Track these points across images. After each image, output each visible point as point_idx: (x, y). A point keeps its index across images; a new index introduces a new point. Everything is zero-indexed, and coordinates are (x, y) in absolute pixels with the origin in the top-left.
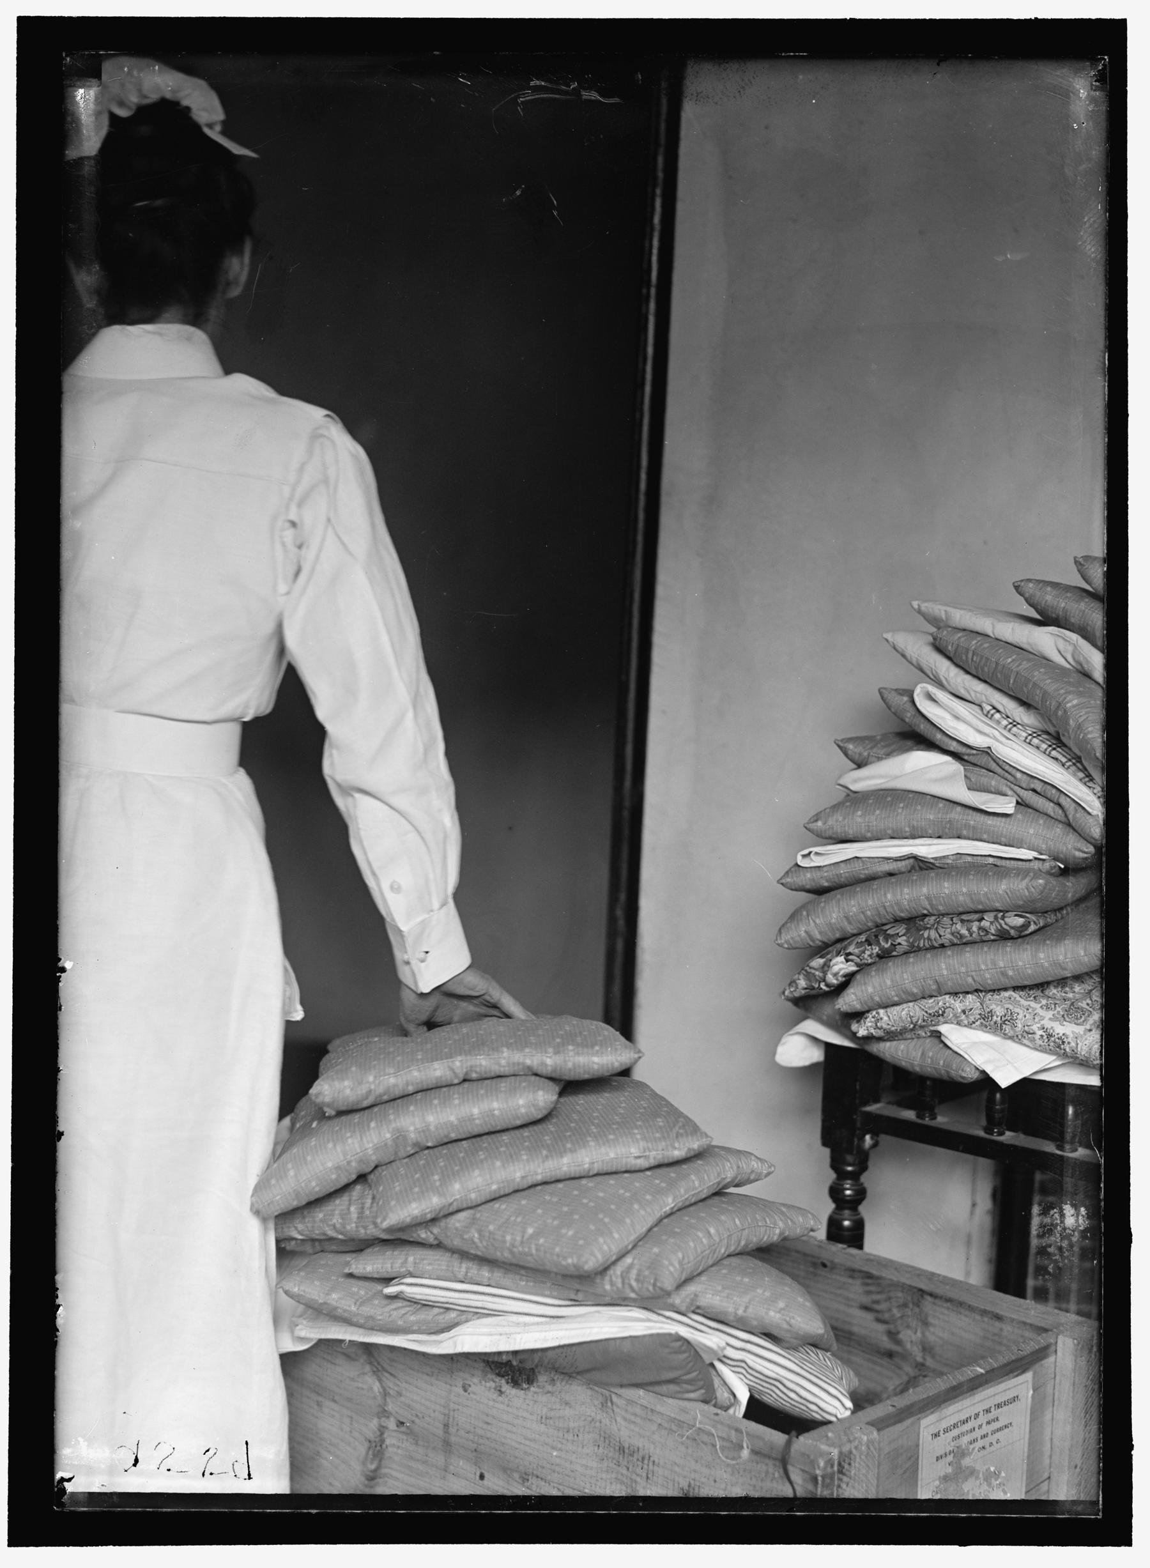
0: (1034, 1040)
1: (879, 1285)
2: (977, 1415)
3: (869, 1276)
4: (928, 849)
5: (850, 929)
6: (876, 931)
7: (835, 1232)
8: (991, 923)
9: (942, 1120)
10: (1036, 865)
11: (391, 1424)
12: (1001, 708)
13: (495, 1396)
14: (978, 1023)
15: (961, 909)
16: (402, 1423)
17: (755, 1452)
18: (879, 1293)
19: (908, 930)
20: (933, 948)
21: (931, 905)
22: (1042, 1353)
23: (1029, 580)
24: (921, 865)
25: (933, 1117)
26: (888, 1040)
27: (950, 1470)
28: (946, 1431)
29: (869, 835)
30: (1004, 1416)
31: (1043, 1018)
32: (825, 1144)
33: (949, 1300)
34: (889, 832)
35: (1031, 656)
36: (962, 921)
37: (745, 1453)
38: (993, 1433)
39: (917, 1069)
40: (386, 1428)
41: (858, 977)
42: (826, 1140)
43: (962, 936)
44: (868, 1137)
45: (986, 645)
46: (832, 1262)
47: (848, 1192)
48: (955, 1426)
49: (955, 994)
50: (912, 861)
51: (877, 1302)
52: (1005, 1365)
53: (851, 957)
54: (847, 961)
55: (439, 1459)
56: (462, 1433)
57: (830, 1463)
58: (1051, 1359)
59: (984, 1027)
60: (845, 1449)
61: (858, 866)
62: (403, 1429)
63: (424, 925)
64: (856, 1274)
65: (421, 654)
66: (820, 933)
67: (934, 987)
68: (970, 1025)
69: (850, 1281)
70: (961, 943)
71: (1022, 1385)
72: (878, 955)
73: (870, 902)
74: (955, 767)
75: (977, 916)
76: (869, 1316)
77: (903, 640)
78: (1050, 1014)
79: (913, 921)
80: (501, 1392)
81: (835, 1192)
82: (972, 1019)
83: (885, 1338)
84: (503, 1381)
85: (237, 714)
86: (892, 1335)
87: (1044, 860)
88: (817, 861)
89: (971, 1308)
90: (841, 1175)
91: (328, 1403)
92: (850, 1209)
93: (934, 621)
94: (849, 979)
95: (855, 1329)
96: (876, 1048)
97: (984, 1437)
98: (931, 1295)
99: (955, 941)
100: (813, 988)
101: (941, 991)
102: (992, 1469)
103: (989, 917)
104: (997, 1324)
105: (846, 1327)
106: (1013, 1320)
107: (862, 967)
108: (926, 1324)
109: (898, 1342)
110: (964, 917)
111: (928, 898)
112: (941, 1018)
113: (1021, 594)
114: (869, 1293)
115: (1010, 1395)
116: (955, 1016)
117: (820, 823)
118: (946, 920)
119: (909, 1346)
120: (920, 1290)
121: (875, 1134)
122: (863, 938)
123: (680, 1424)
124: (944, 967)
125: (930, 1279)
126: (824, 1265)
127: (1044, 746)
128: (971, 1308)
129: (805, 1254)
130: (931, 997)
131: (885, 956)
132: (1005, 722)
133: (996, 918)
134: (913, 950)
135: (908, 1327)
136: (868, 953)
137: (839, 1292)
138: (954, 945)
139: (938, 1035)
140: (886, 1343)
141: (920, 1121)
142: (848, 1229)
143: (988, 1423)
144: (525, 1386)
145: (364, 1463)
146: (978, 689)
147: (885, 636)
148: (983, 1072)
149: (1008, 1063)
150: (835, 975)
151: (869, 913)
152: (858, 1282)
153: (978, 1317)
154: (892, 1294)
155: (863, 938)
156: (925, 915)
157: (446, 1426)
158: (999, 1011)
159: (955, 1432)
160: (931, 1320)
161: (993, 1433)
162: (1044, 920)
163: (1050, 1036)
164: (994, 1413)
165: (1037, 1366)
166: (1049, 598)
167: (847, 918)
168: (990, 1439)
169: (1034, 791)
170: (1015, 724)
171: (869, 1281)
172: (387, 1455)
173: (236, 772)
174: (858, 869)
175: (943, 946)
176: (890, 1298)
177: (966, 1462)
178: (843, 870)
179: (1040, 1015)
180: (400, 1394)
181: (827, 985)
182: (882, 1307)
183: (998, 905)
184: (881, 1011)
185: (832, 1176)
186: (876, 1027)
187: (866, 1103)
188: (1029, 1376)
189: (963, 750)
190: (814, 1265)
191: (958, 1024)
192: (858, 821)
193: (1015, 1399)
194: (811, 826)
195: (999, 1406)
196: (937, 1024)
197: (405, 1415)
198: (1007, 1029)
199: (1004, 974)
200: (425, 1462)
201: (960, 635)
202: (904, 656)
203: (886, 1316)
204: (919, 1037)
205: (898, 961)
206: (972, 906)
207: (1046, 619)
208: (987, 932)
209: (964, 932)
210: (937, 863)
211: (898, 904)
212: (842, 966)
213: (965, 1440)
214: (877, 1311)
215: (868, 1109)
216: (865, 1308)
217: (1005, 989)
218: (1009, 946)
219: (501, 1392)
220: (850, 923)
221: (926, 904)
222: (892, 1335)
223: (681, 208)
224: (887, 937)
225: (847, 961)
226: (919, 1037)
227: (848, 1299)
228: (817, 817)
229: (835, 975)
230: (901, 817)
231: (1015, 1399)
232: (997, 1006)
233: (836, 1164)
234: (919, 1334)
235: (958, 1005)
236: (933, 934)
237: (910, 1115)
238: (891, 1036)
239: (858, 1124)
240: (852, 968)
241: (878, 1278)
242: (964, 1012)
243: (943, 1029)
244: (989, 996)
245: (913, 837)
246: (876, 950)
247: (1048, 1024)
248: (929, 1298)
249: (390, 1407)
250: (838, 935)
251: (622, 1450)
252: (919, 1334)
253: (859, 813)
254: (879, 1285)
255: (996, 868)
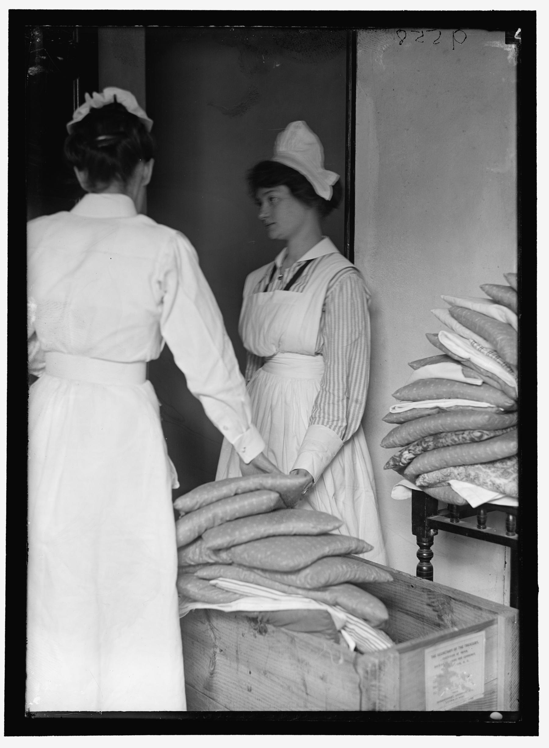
0: (487, 486)
1: (434, 595)
2: (455, 649)
3: (430, 591)
4: (444, 404)
5: (411, 439)
6: (421, 440)
7: (420, 572)
8: (468, 435)
9: (461, 523)
10: (489, 410)
11: (218, 651)
12: (476, 341)
13: (253, 638)
14: (464, 479)
15: (455, 430)
16: (222, 651)
17: (346, 661)
18: (434, 598)
19: (434, 439)
20: (444, 447)
21: (443, 428)
22: (490, 623)
23: (487, 285)
24: (441, 411)
25: (458, 522)
26: (431, 487)
27: (442, 672)
28: (439, 655)
29: (419, 398)
30: (470, 650)
31: (491, 476)
32: (414, 534)
33: (461, 601)
34: (427, 397)
35: (487, 318)
36: (456, 435)
37: (341, 661)
38: (465, 657)
39: (443, 500)
40: (216, 652)
41: (415, 460)
42: (415, 531)
43: (455, 441)
44: (432, 530)
45: (469, 314)
46: (415, 585)
47: (425, 555)
48: (444, 653)
49: (455, 466)
50: (437, 409)
51: (433, 602)
52: (469, 628)
53: (411, 451)
54: (409, 453)
55: (234, 665)
56: (242, 654)
57: (374, 665)
58: (495, 626)
59: (467, 481)
60: (382, 659)
61: (415, 412)
62: (222, 653)
63: (241, 440)
64: (425, 590)
65: (224, 328)
66: (399, 441)
67: (445, 464)
68: (462, 480)
69: (422, 593)
70: (456, 444)
71: (480, 637)
72: (422, 450)
73: (418, 427)
74: (459, 367)
75: (461, 432)
76: (431, 609)
77: (437, 312)
78: (494, 475)
79: (436, 435)
80: (255, 637)
81: (419, 555)
82: (462, 477)
83: (437, 618)
84: (256, 632)
85: (142, 358)
86: (440, 617)
87: (493, 407)
88: (398, 411)
89: (470, 605)
90: (422, 547)
91: (196, 642)
92: (425, 562)
93: (450, 303)
94: (411, 460)
95: (425, 614)
96: (431, 492)
97: (460, 658)
98: (454, 599)
99: (453, 443)
100: (396, 465)
101: (448, 466)
102: (465, 673)
103: (466, 433)
104: (480, 612)
105: (422, 613)
106: (486, 610)
107: (416, 456)
108: (452, 612)
109: (442, 620)
110: (457, 433)
111: (442, 425)
112: (449, 477)
113: (484, 290)
114: (430, 598)
115: (474, 640)
116: (455, 476)
117: (398, 394)
118: (449, 434)
119: (446, 622)
120: (450, 597)
121: (436, 529)
122: (416, 443)
123: (319, 649)
124: (448, 455)
125: (453, 592)
126: (412, 587)
127: (494, 357)
128: (470, 605)
129: (405, 582)
130: (445, 468)
131: (425, 450)
132: (478, 347)
133: (469, 433)
134: (436, 448)
135: (446, 613)
136: (417, 449)
137: (418, 598)
138: (453, 445)
139: (449, 485)
140: (437, 620)
141: (451, 523)
142: (425, 571)
143: (462, 652)
144: (264, 634)
145: (209, 668)
146: (467, 333)
147: (432, 311)
148: (466, 501)
149: (474, 495)
150: (405, 459)
151: (418, 432)
152: (426, 594)
153: (472, 609)
154: (439, 599)
155: (416, 443)
156: (442, 433)
157: (237, 651)
158: (473, 474)
159: (444, 656)
160: (454, 610)
161: (465, 657)
162: (497, 433)
163: (494, 484)
164: (465, 649)
165: (488, 629)
166: (495, 292)
167: (409, 434)
168: (463, 660)
169: (488, 376)
170: (482, 348)
171: (429, 593)
172: (217, 664)
173: (145, 382)
174: (415, 413)
175: (448, 446)
176: (438, 601)
177: (451, 669)
178: (409, 414)
179: (490, 474)
180: (220, 638)
181: (402, 463)
182: (435, 604)
183: (470, 427)
184: (426, 475)
185: (418, 548)
186: (424, 482)
187: (430, 515)
188: (483, 633)
189: (460, 359)
190: (408, 586)
191: (457, 479)
192: (414, 393)
193: (475, 643)
194: (395, 395)
195: (467, 645)
196: (448, 480)
197: (223, 647)
198: (476, 481)
199: (473, 458)
200: (230, 667)
201: (459, 309)
202: (439, 319)
203: (437, 608)
204: (443, 486)
205: (430, 452)
206: (460, 428)
207: (496, 301)
208: (466, 440)
209: (456, 439)
210: (447, 409)
211: (429, 428)
212: (407, 455)
213: (449, 660)
214: (433, 606)
215: (431, 518)
216: (429, 605)
217: (477, 464)
218: (475, 446)
219: (255, 637)
220: (411, 437)
221: (441, 427)
222: (440, 617)
223: (357, 127)
224: (426, 442)
225: (409, 453)
226: (443, 486)
227: (422, 601)
228: (397, 392)
229: (405, 459)
230: (431, 390)
231: (475, 643)
232: (472, 471)
233: (419, 543)
234: (450, 616)
235: (456, 471)
236: (443, 440)
237: (448, 520)
238: (430, 486)
239: (426, 525)
240: (412, 456)
241: (434, 592)
242: (458, 474)
243: (451, 482)
244: (469, 467)
245: (430, 399)
246: (421, 448)
247: (493, 479)
248: (453, 600)
249: (217, 643)
250: (406, 442)
251: (299, 660)
252: (450, 616)
253: (415, 389)
254: (434, 595)
255: (472, 411)
